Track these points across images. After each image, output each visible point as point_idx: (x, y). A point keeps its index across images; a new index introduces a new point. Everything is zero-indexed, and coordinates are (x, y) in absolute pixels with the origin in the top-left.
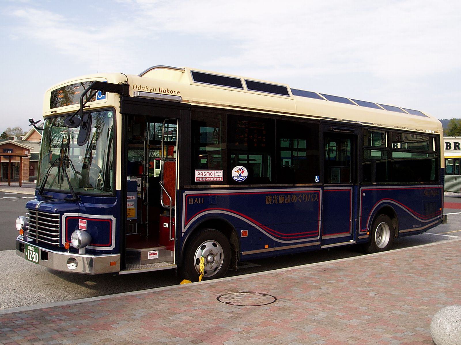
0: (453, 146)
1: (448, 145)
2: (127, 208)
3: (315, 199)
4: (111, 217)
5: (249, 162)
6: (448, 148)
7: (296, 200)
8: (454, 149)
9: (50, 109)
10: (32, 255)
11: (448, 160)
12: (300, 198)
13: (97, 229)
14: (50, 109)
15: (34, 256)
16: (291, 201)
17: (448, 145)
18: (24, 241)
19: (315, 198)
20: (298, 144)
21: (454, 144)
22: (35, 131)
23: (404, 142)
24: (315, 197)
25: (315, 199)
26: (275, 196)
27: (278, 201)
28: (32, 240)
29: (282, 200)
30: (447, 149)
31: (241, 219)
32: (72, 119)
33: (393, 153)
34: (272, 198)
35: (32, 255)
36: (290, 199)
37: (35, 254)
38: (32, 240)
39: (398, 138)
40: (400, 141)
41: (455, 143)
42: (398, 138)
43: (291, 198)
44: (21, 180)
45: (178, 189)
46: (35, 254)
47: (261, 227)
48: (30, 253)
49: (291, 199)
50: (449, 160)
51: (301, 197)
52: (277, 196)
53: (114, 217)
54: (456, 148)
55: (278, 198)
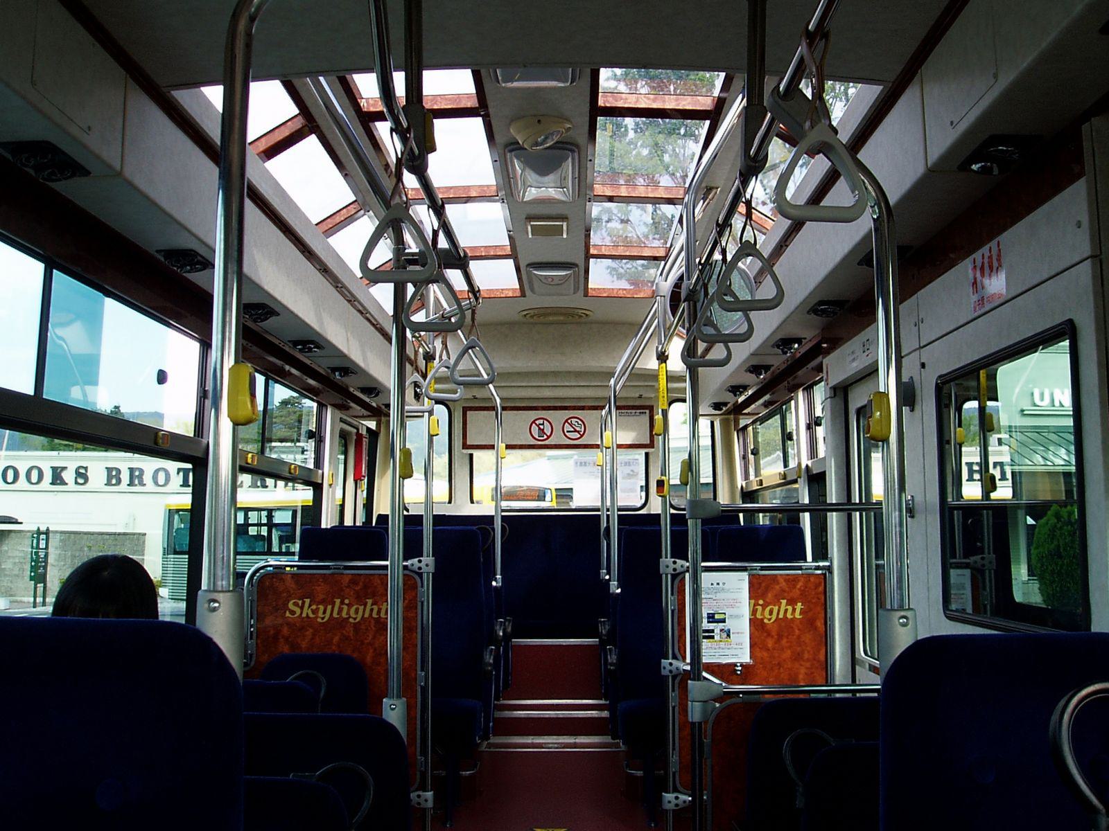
0: (125, 477)
1: (114, 473)
6: (114, 481)
8: (51, 484)
11: (179, 515)
17: (114, 473)
21: (108, 471)
22: (987, 500)
23: (751, 457)
28: (744, 412)
30: (109, 484)
33: (346, 524)
38: (744, 412)
39: (542, 431)
40: (546, 442)
41: (132, 470)
42: (542, 431)
44: (270, 458)
47: (701, 283)
50: (181, 513)
54: (256, 483)
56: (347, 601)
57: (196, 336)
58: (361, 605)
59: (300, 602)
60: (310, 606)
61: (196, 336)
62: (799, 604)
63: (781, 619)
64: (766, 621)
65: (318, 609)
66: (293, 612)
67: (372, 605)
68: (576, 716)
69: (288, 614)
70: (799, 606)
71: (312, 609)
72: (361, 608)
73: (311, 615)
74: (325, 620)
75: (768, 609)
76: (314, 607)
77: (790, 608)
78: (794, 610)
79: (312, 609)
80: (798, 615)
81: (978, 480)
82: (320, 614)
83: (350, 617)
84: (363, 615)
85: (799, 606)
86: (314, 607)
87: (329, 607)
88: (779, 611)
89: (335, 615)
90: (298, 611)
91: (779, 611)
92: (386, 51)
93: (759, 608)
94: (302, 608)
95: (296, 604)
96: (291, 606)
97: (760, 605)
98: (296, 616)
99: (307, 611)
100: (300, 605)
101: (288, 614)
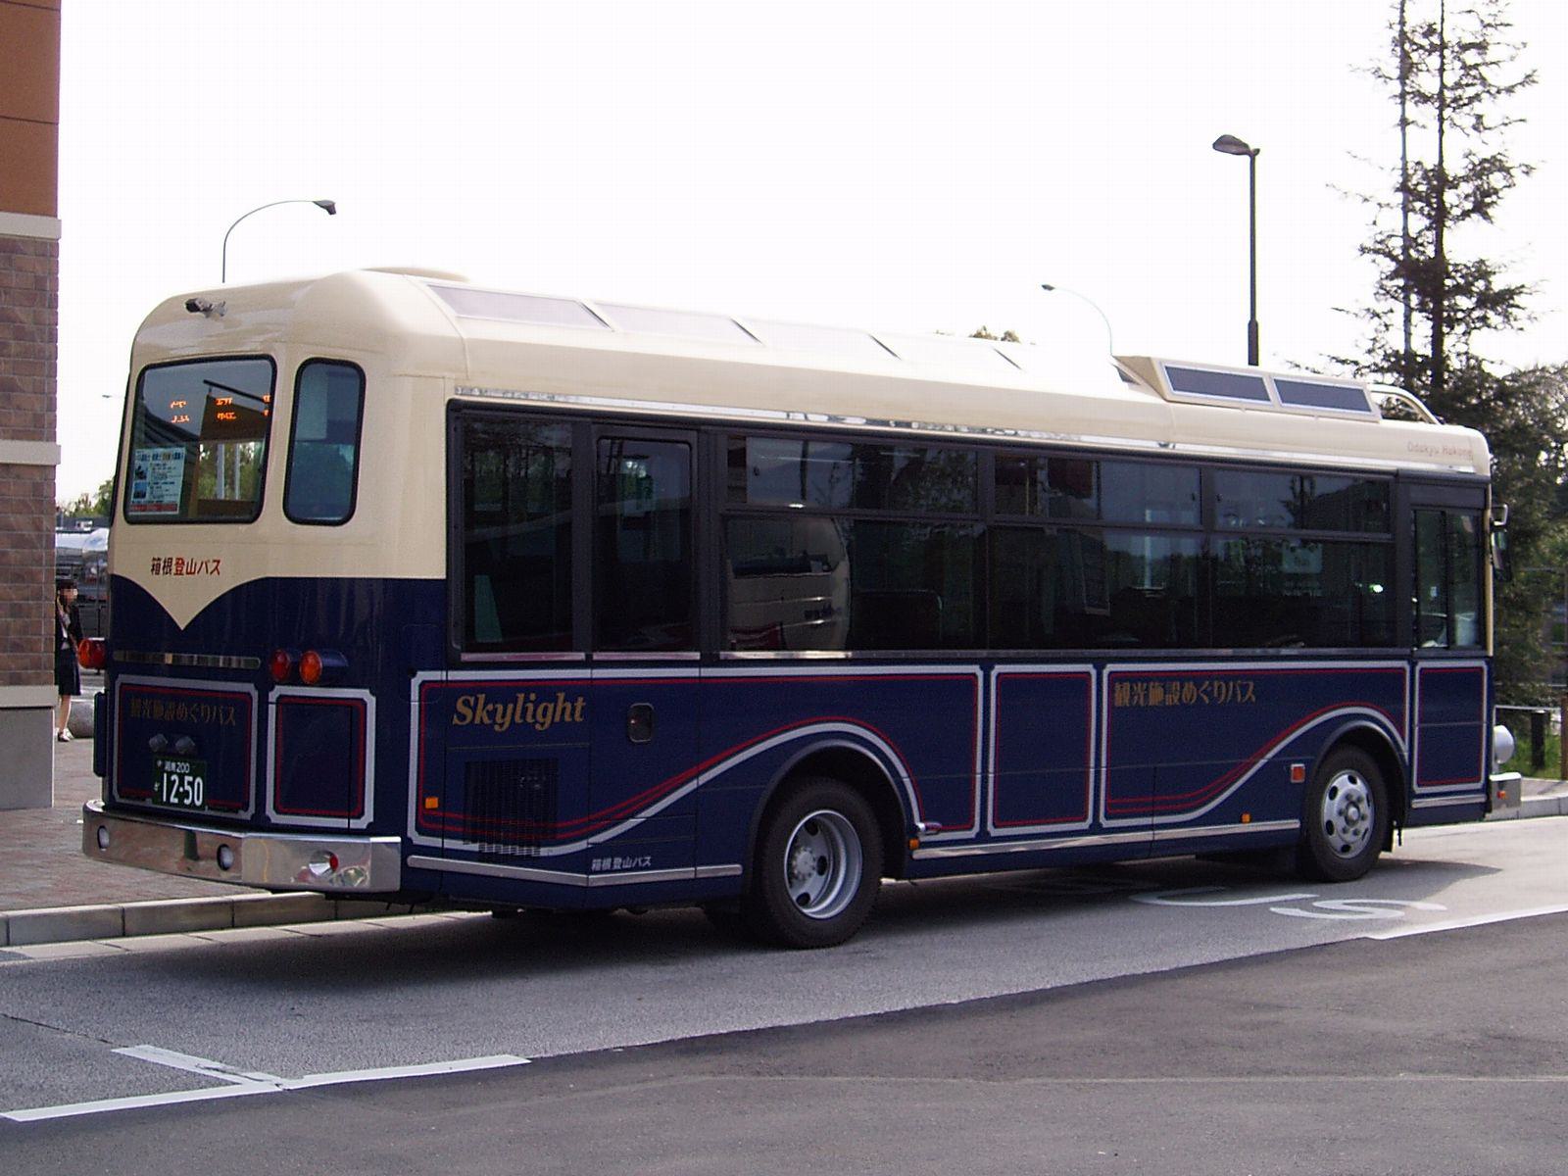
2: (104, 688)
3: (1247, 697)
4: (364, 694)
5: (591, 656)
7: (1195, 697)
9: (454, 408)
10: (182, 784)
12: (1205, 691)
13: (90, 570)
14: (454, 408)
15: (188, 788)
16: (1180, 699)
18: (969, 432)
19: (1246, 693)
20: (441, 676)
24: (1248, 690)
25: (1247, 697)
26: (1139, 685)
27: (1146, 696)
29: (1156, 696)
31: (346, 690)
32: (478, 507)
34: (1131, 687)
35: (182, 784)
36: (1178, 694)
37: (191, 784)
43: (1181, 692)
45: (697, 656)
46: (191, 784)
48: (171, 784)
49: (1181, 696)
51: (1209, 689)
52: (1145, 685)
53: (372, 693)
55: (1147, 689)
56: (533, 697)
57: (841, 655)
58: (551, 703)
59: (472, 700)
60: (486, 704)
61: (841, 655)
62: (580, 699)
63: (557, 723)
64: (538, 727)
65: (496, 710)
66: (463, 717)
67: (564, 702)
68: (623, 882)
69: (456, 721)
70: (580, 703)
71: (488, 711)
72: (551, 706)
73: (487, 721)
74: (546, 726)
75: (542, 706)
76: (490, 707)
77: (569, 705)
78: (574, 709)
79: (488, 711)
80: (578, 718)
81: (266, 403)
82: (499, 720)
83: (537, 722)
84: (553, 717)
85: (580, 703)
86: (490, 707)
87: (511, 706)
88: (513, 714)
89: (518, 720)
90: (469, 713)
91: (513, 714)
92: (695, 460)
93: (531, 706)
94: (474, 710)
95: (466, 703)
96: (460, 706)
97: (531, 702)
98: (464, 723)
99: (482, 715)
100: (472, 703)
101: (456, 721)
